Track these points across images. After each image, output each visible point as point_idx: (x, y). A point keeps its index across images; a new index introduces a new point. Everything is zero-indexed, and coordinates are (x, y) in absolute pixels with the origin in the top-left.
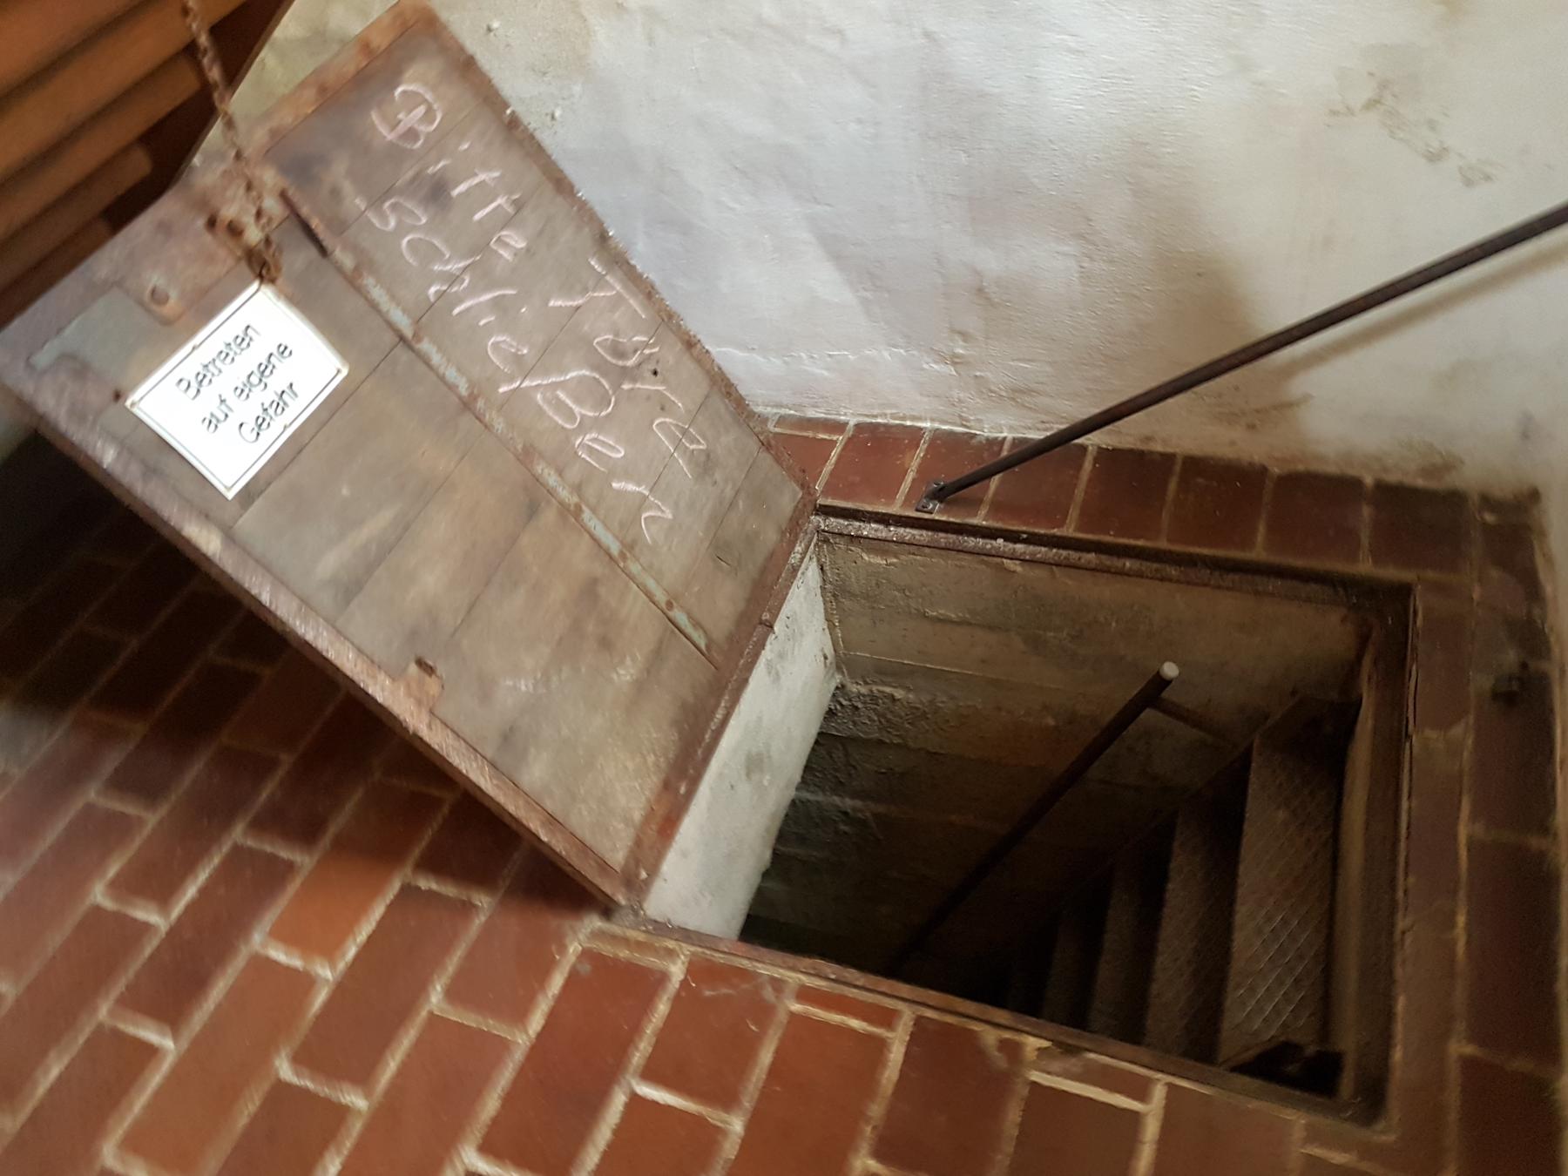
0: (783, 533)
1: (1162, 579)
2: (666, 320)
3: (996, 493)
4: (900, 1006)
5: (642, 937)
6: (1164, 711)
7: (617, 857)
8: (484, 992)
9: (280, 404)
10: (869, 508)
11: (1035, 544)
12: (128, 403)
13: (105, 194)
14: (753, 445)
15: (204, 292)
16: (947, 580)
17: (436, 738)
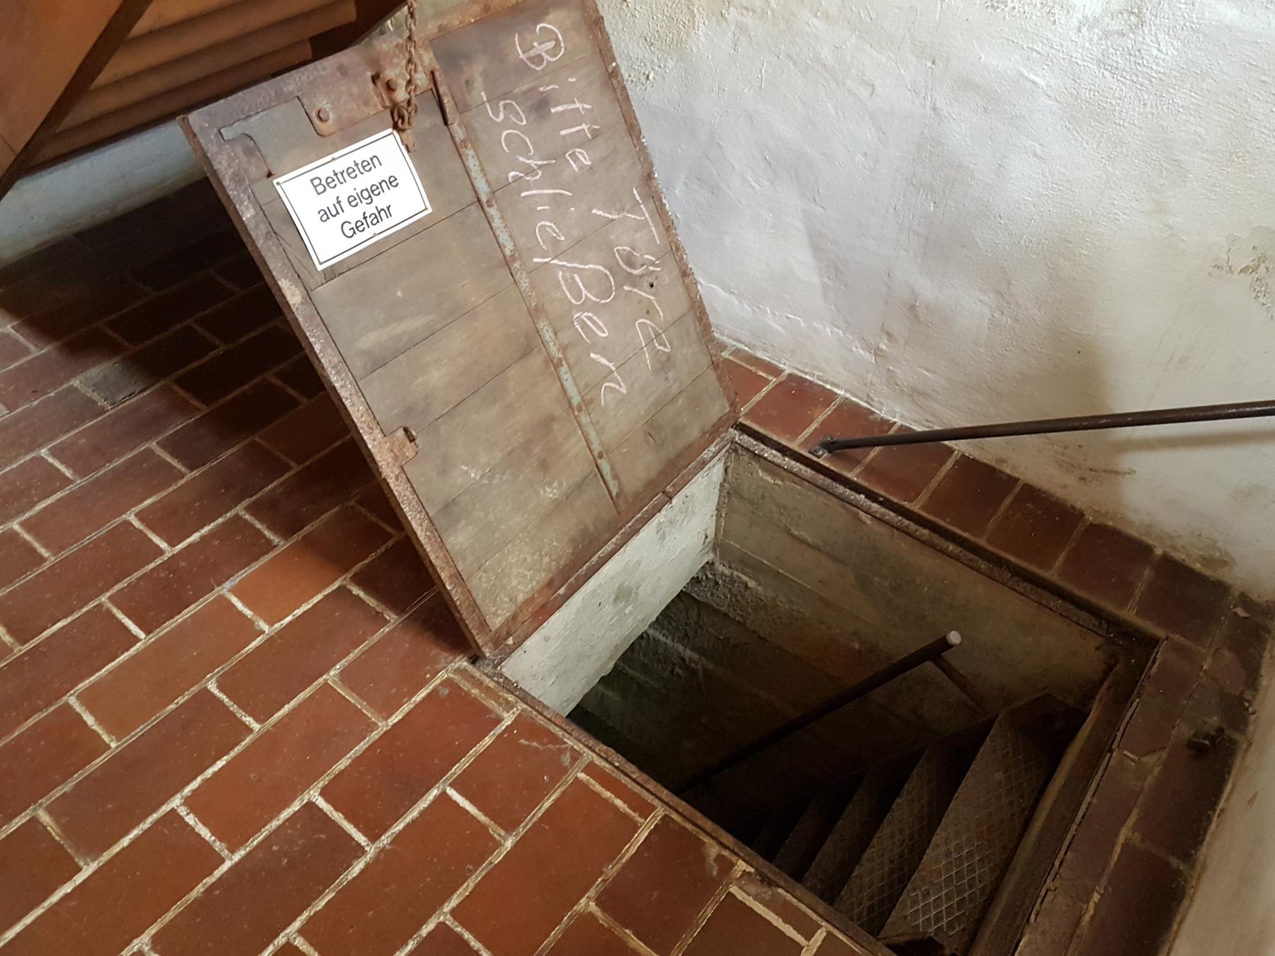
0: (704, 433)
1: (972, 568)
2: (675, 250)
3: (872, 460)
4: (656, 802)
5: (492, 685)
6: (941, 668)
7: (496, 623)
8: (369, 687)
9: (377, 218)
10: (775, 438)
11: (886, 507)
12: (275, 182)
13: (318, 26)
14: (705, 361)
15: (354, 123)
16: (816, 514)
17: (398, 488)
